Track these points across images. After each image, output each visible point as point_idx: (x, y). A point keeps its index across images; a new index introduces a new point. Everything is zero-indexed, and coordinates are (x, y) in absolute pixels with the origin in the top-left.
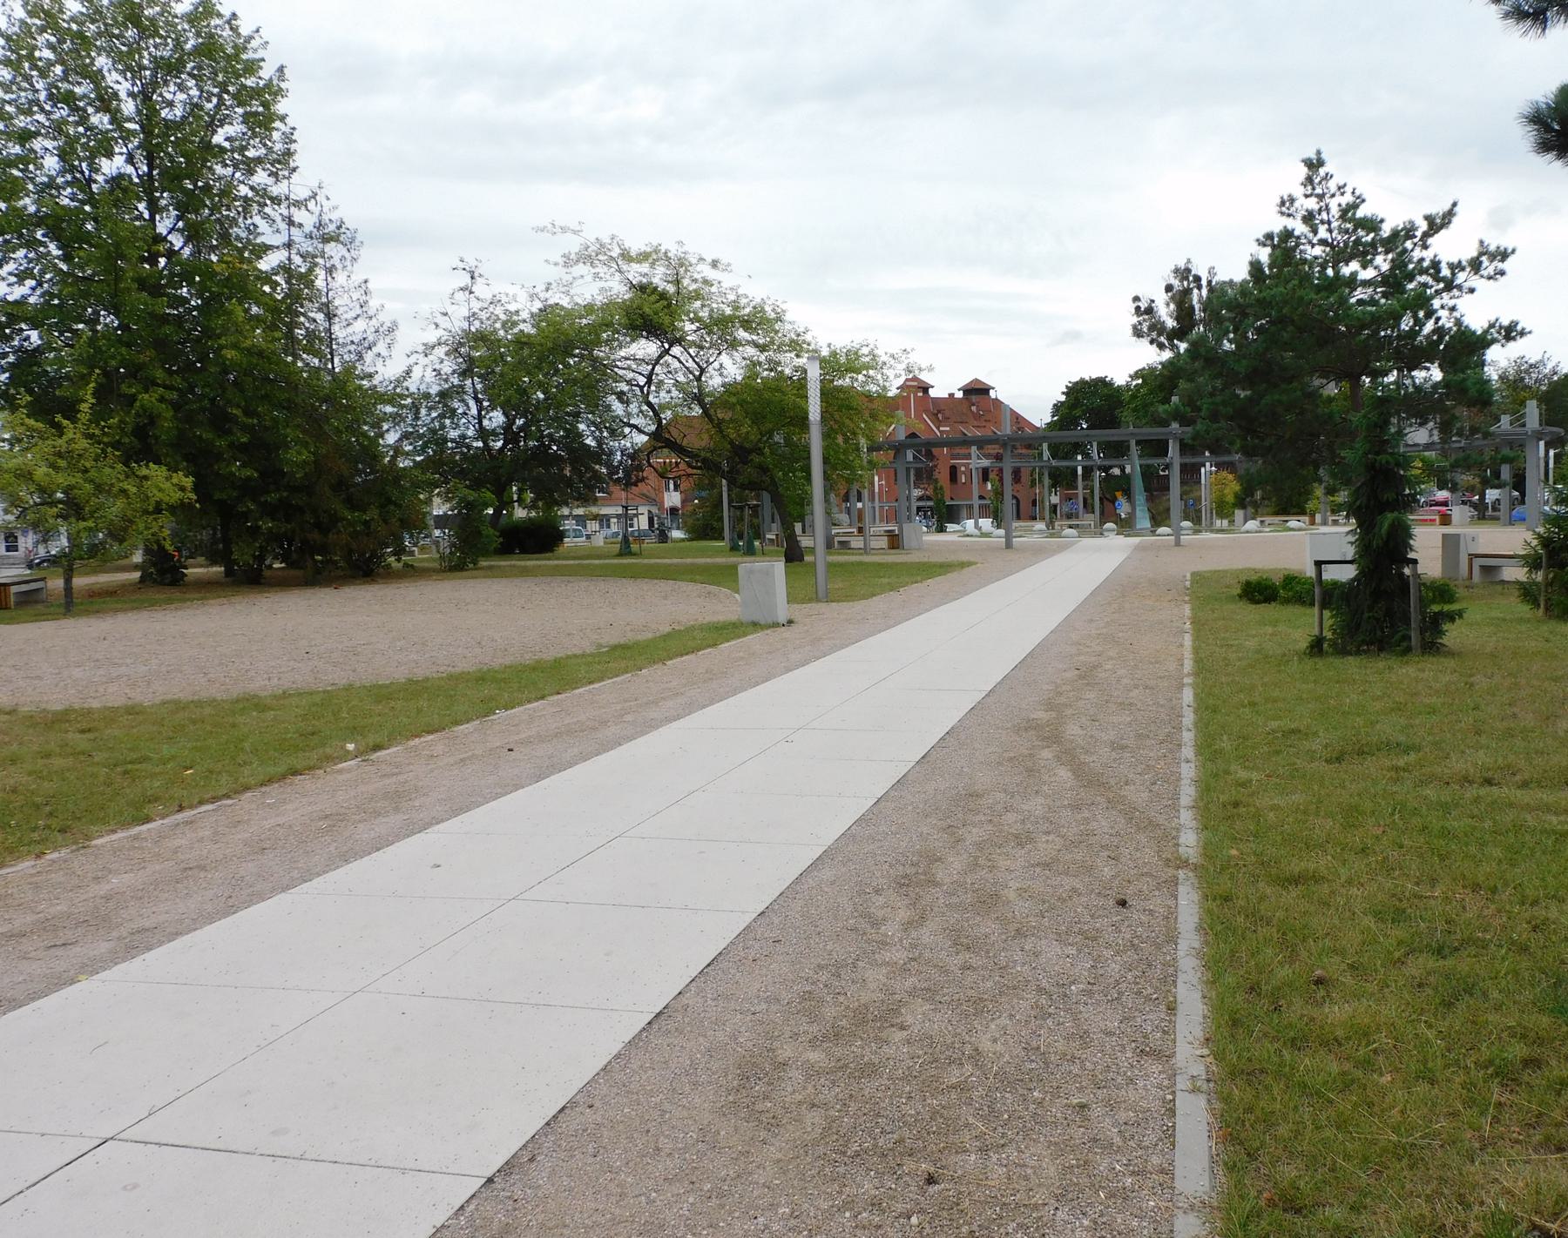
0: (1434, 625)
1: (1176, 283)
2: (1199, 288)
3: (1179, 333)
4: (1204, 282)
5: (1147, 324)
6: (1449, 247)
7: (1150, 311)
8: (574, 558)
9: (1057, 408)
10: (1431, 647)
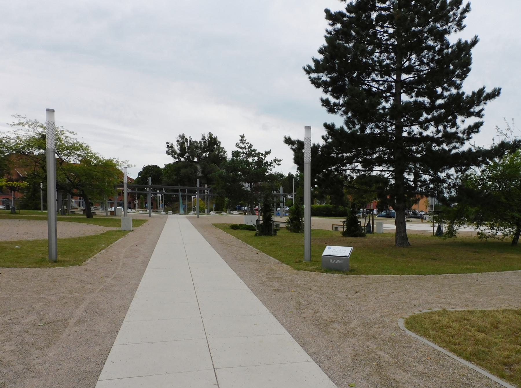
0: (275, 231)
1: (180, 140)
2: (187, 142)
3: (182, 155)
4: (188, 141)
5: (171, 150)
6: (269, 159)
7: (172, 147)
8: (73, 218)
9: (140, 173)
10: (275, 235)
